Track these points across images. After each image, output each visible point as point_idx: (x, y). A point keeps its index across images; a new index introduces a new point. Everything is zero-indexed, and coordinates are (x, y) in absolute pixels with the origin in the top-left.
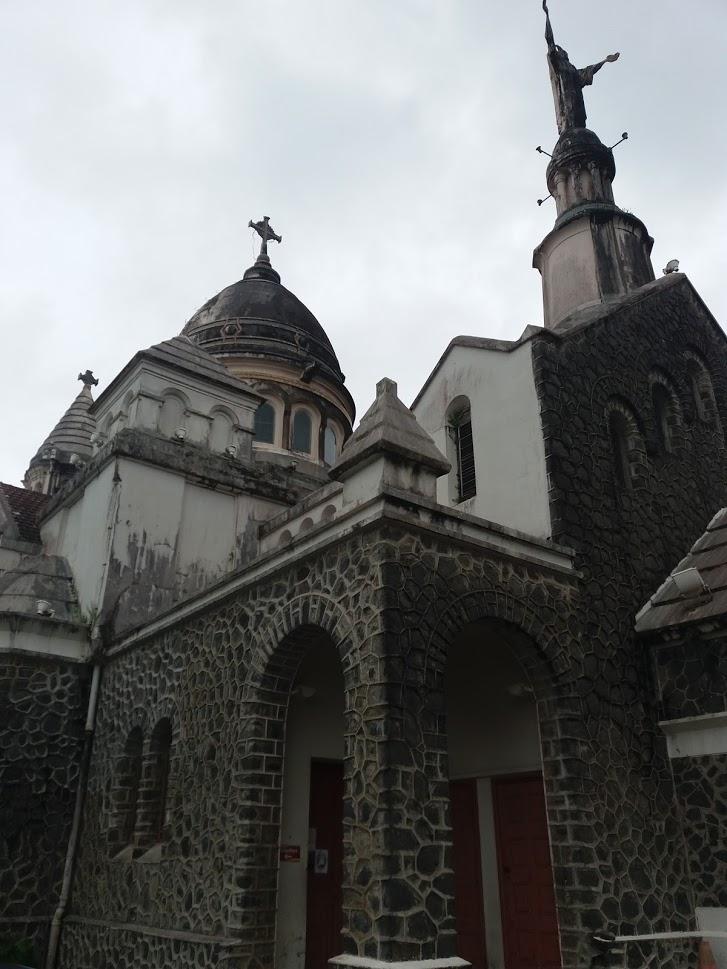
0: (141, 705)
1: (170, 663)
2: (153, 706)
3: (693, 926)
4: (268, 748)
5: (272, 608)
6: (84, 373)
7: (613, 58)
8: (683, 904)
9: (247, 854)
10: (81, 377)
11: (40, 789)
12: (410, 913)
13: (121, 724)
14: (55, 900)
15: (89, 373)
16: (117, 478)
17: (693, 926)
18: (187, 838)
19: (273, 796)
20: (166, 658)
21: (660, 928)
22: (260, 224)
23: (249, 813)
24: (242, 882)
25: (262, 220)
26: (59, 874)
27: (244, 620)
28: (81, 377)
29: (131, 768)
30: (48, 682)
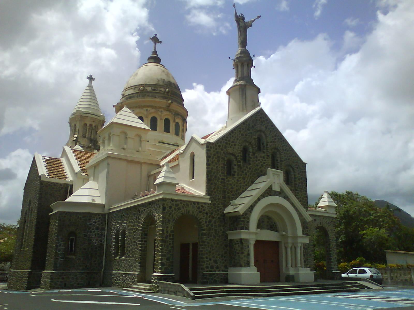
0: (118, 225)
1: (124, 217)
2: (121, 226)
3: (228, 271)
4: (144, 238)
5: (144, 210)
6: (89, 76)
7: (259, 17)
8: (226, 267)
9: (140, 258)
10: (88, 78)
11: (89, 236)
12: (164, 267)
13: (114, 229)
14: (102, 268)
15: (91, 76)
16: (108, 164)
17: (228, 271)
18: (129, 255)
19: (146, 247)
20: (124, 215)
21: (219, 271)
22: (153, 37)
23: (141, 250)
24: (139, 263)
25: (154, 36)
26: (102, 262)
27: (139, 211)
28: (88, 78)
29: (117, 238)
30: (96, 218)
